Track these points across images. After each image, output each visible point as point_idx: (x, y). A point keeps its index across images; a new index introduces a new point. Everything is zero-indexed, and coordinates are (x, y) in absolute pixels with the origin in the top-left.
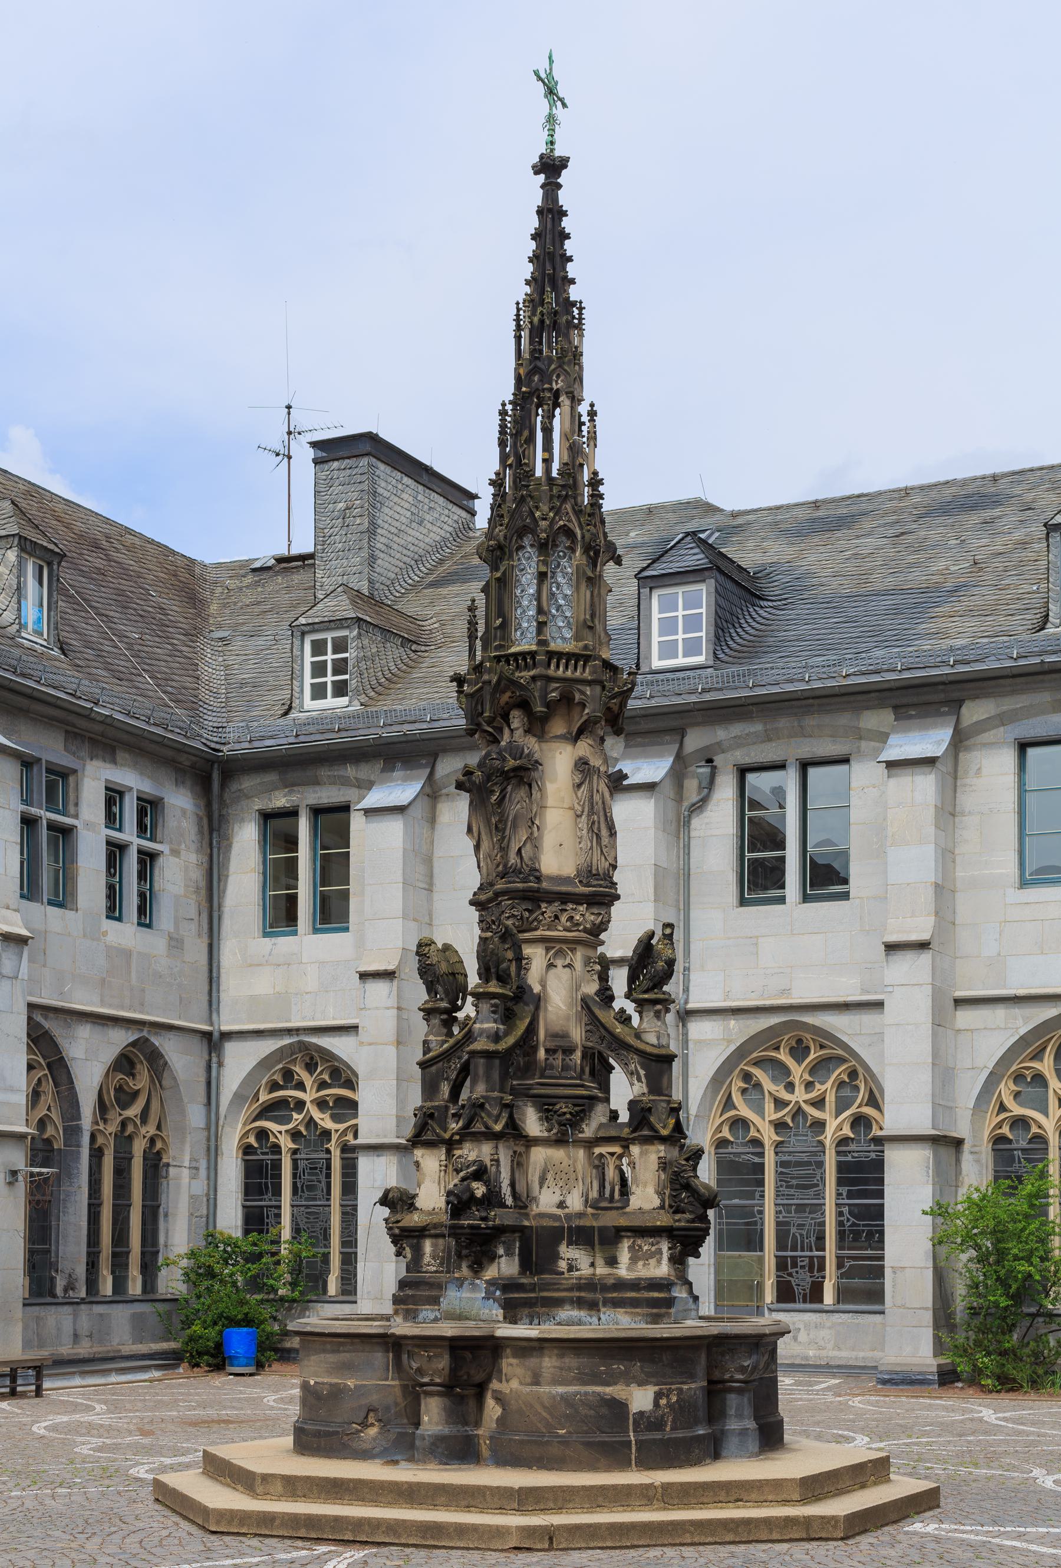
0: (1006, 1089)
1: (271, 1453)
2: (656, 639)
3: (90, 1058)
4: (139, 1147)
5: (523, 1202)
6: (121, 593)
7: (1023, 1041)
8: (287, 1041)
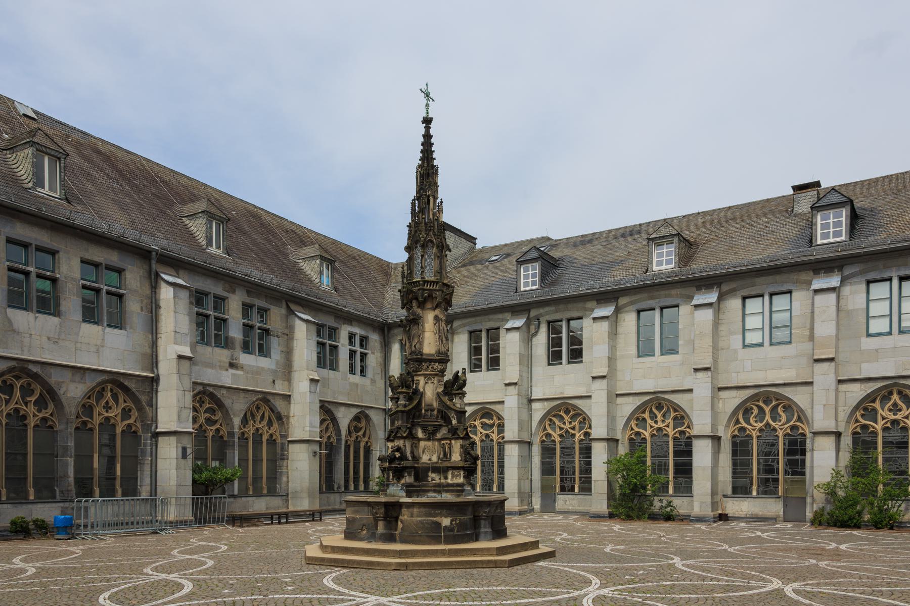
0: (633, 423)
1: (338, 540)
2: (522, 281)
3: (344, 418)
4: (362, 445)
5: (416, 459)
6: (361, 273)
7: (639, 407)
8: (879, 384)
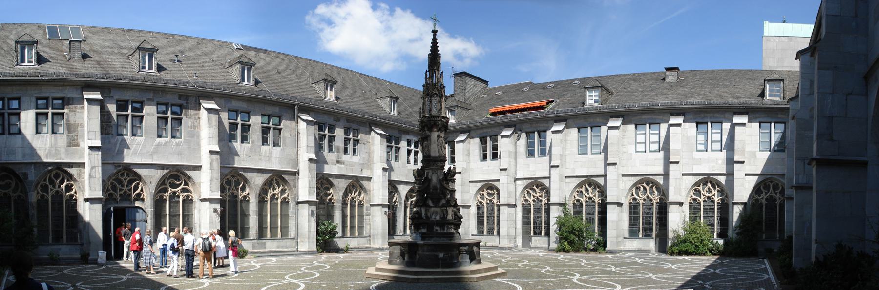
0: (575, 193)
8: (702, 177)
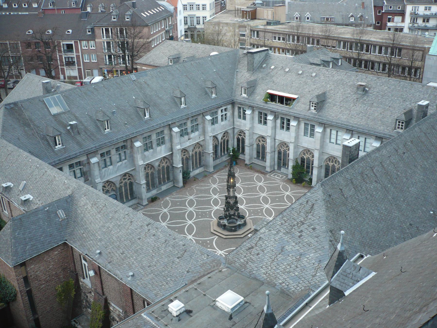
0: (302, 153)
